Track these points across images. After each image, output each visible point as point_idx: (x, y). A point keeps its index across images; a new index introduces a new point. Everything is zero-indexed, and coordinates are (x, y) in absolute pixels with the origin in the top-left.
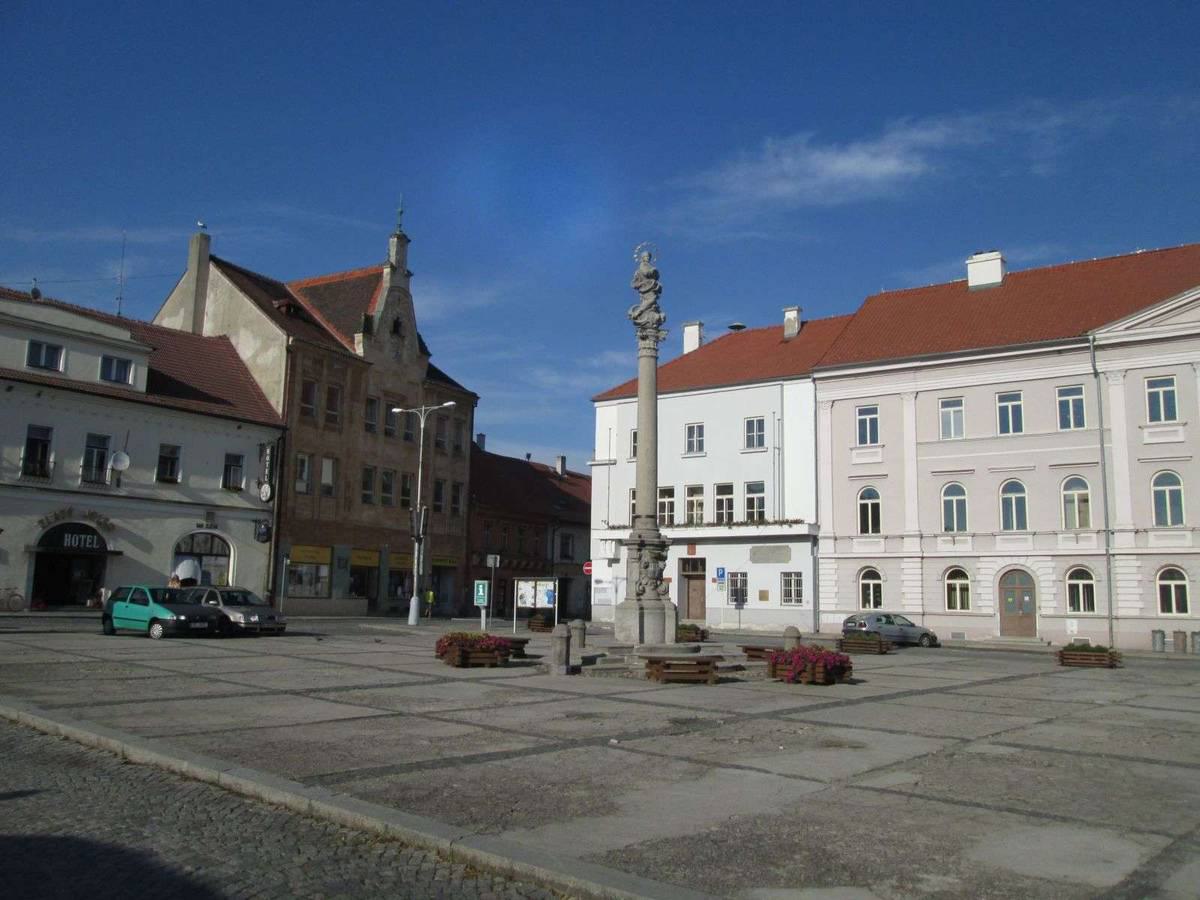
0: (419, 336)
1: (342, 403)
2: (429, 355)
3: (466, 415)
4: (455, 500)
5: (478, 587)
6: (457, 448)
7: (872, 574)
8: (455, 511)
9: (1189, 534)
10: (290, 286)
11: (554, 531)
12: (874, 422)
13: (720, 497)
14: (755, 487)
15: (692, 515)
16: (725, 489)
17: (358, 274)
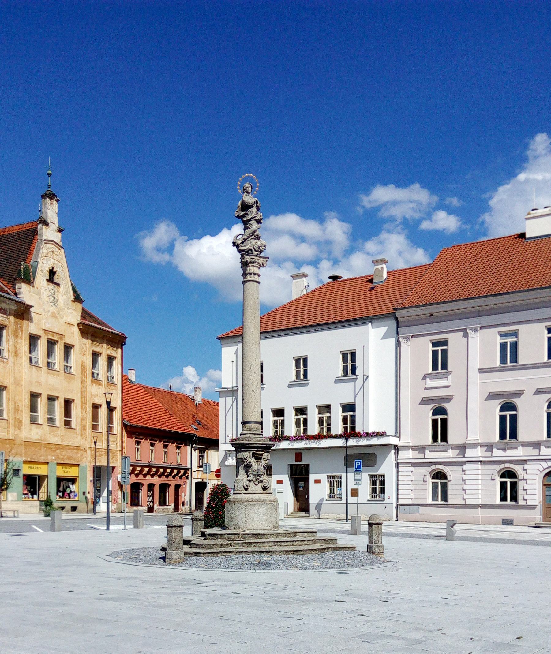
1: (8, 340)
7: (510, 474)
8: (51, 421)
9: (520, 448)
12: (445, 352)
13: (320, 416)
14: (349, 408)
15: (347, 427)
16: (326, 409)
17: (17, 229)
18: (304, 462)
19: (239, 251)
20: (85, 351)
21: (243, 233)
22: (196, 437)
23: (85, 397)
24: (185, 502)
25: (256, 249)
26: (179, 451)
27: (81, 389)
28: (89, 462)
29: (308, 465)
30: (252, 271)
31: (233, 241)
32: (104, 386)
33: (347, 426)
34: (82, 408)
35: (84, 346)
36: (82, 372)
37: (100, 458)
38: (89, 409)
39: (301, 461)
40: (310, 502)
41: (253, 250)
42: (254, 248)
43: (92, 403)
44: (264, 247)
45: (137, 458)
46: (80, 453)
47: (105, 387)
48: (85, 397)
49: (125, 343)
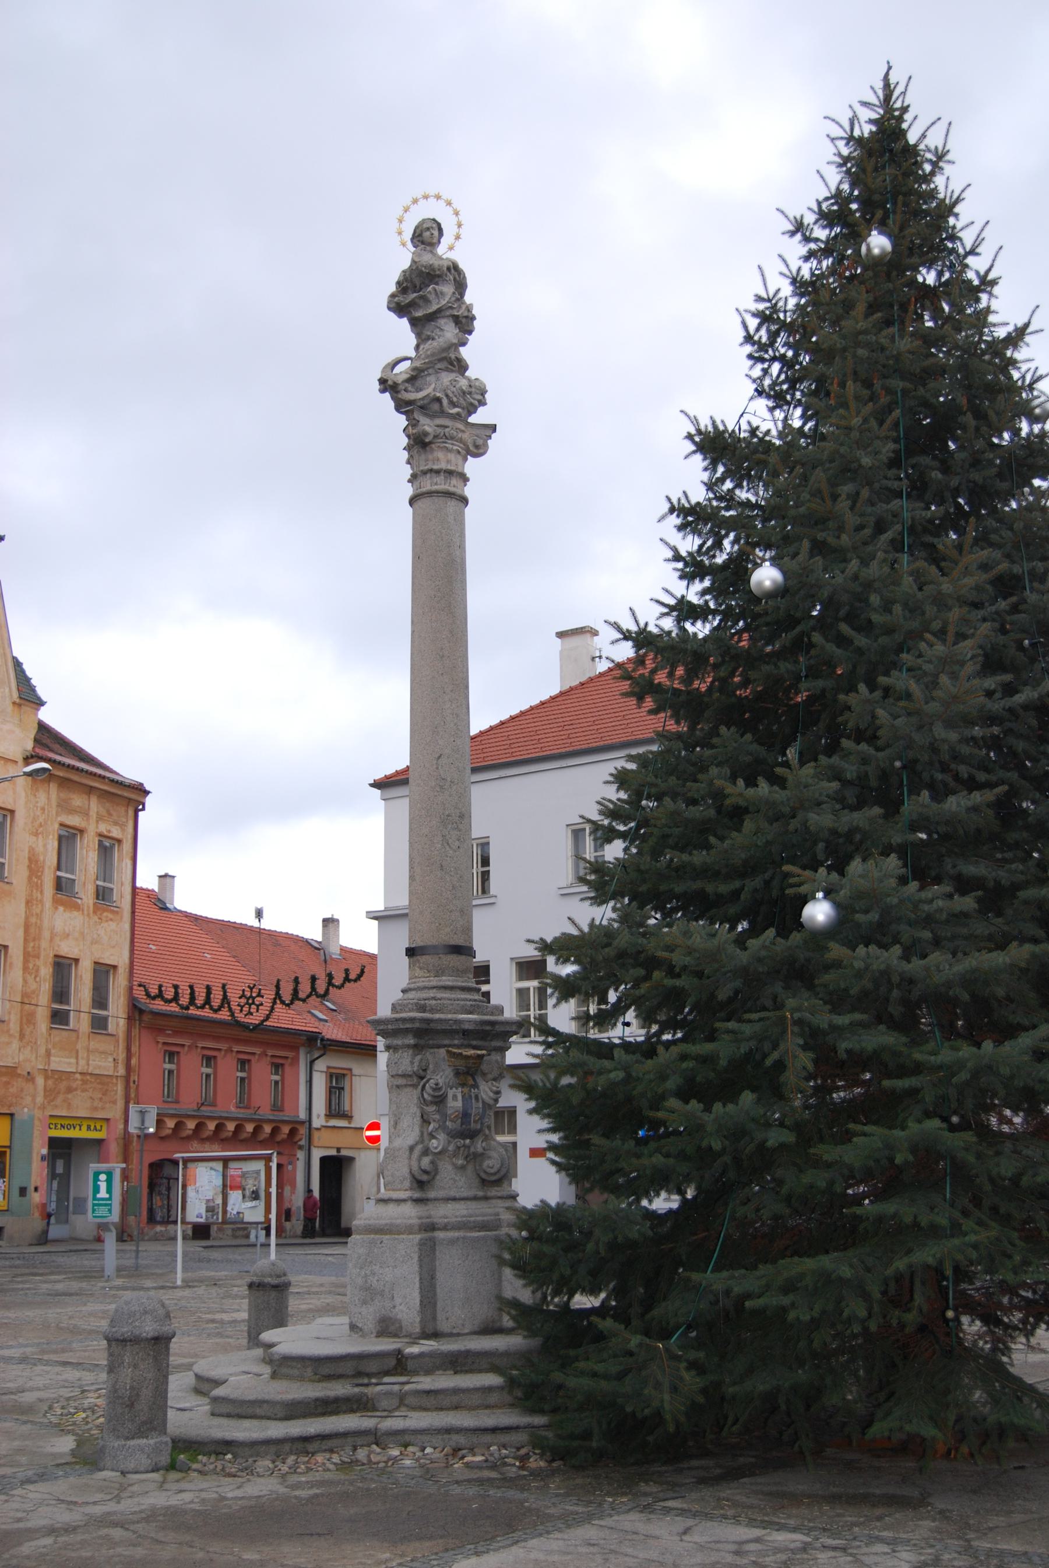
0: (17, 664)
2: (41, 703)
3: (122, 826)
4: (100, 1000)
5: (96, 1179)
6: (102, 895)
8: (99, 1024)
10: (945, 1196)
11: (312, 1062)
19: (401, 406)
20: (41, 825)
21: (413, 354)
22: (322, 1039)
23: (37, 938)
24: (293, 1209)
25: (455, 399)
26: (173, 1067)
27: (27, 918)
28: (39, 1108)
30: (443, 465)
31: (379, 377)
34: (25, 969)
35: (39, 813)
36: (30, 878)
37: (70, 1096)
38: (46, 971)
41: (445, 401)
42: (447, 396)
43: (51, 955)
44: (480, 397)
46: (19, 1083)
48: (34, 940)
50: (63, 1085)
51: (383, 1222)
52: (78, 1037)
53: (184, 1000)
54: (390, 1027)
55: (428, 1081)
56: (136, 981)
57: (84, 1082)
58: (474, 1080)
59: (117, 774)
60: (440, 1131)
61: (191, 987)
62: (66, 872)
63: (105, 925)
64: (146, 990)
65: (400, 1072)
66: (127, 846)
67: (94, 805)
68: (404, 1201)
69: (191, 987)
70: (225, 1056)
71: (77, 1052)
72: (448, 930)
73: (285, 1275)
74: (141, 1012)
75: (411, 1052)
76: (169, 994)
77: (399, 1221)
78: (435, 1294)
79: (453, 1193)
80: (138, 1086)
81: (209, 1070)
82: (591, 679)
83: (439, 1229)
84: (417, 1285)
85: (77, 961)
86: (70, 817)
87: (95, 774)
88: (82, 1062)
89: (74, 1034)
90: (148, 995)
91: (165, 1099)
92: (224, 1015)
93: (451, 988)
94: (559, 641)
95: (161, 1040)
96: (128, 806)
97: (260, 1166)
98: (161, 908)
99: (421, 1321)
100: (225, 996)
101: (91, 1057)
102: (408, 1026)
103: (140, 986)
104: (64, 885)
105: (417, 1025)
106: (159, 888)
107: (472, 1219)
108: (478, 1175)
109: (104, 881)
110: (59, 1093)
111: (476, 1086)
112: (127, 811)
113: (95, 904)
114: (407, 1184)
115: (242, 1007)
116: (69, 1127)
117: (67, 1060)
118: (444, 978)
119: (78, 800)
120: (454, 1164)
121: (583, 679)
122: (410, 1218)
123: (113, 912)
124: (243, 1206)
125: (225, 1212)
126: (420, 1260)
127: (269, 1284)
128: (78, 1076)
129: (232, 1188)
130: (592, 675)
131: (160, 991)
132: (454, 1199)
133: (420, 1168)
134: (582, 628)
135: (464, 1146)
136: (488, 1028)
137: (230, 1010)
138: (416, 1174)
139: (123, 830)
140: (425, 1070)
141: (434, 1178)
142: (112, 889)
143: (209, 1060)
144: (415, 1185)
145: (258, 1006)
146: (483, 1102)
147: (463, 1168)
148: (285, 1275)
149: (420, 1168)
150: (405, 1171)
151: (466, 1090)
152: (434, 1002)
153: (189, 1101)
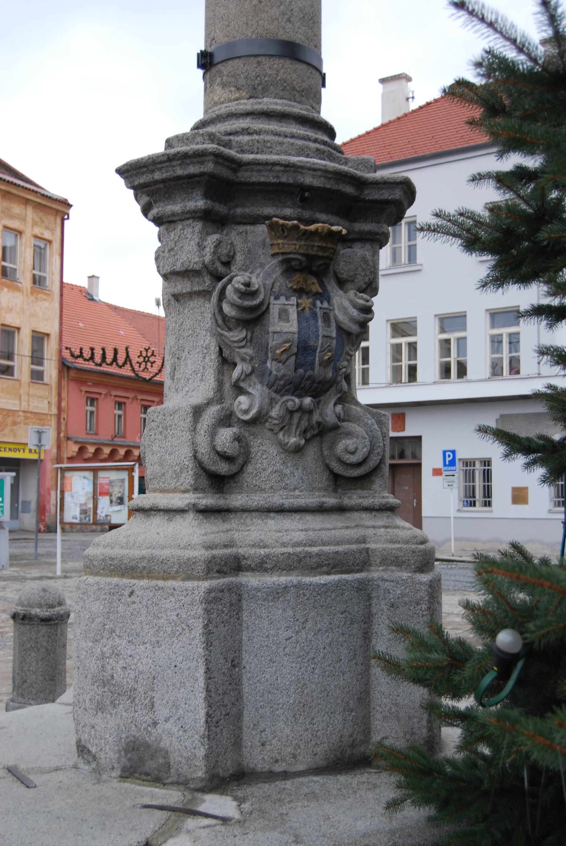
3: (52, 231)
8: (37, 376)
18: (410, 431)
26: (93, 409)
29: (418, 439)
32: (25, 293)
33: (499, 356)
37: (15, 428)
39: (403, 429)
40: (424, 514)
45: (90, 430)
47: (27, 295)
49: (68, 215)
50: (9, 420)
51: (136, 553)
52: (20, 385)
53: (98, 359)
54: (157, 176)
55: (230, 281)
56: (64, 345)
57: (26, 418)
58: (322, 284)
59: (47, 191)
60: (254, 378)
61: (103, 350)
62: (11, 263)
63: (40, 303)
64: (71, 352)
65: (178, 267)
66: (56, 245)
67: (30, 213)
68: (181, 511)
69: (103, 350)
70: (132, 402)
71: (20, 396)
72: (275, 12)
73: (60, 604)
74: (69, 368)
75: (199, 226)
76: (87, 354)
77: (166, 553)
78: (239, 697)
79: (277, 499)
80: (66, 424)
81: (120, 412)
82: (406, 115)
83: (250, 569)
84: (201, 683)
85: (19, 329)
86: (11, 222)
87: (29, 190)
88: (24, 404)
89: (17, 383)
90: (72, 355)
91: (88, 431)
92: (126, 372)
93: (282, 117)
94: (381, 86)
95: (84, 389)
96: (56, 215)
97: (124, 475)
98: (89, 299)
99: (206, 756)
100: (128, 356)
101: (31, 400)
102: (193, 169)
103: (67, 348)
104: (8, 273)
105: (209, 167)
106: (89, 286)
107: (315, 549)
108: (327, 467)
109: (40, 271)
110: (7, 425)
111: (324, 296)
112: (55, 219)
113: (32, 288)
114: (188, 479)
115: (140, 364)
116: (15, 450)
117: (13, 402)
118: (265, 100)
119: (17, 209)
120: (283, 446)
121: (400, 114)
122: (189, 546)
123: (46, 294)
124: (111, 510)
125: (95, 513)
126: (208, 632)
127: (36, 616)
128: (21, 413)
129: (101, 494)
130: (406, 111)
131: (81, 352)
132: (281, 511)
133: (214, 448)
134: (399, 75)
135: (300, 409)
136: (349, 190)
137: (132, 366)
138: (205, 459)
139: (53, 234)
140: (227, 264)
141: (241, 470)
142: (45, 278)
143: (120, 405)
144: (204, 482)
145: (141, 355)
146: (340, 329)
147: (298, 450)
148: (60, 604)
149: (214, 448)
150: (185, 453)
151: (306, 302)
152: (247, 138)
153: (105, 435)
